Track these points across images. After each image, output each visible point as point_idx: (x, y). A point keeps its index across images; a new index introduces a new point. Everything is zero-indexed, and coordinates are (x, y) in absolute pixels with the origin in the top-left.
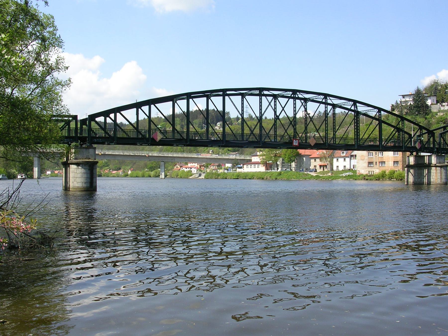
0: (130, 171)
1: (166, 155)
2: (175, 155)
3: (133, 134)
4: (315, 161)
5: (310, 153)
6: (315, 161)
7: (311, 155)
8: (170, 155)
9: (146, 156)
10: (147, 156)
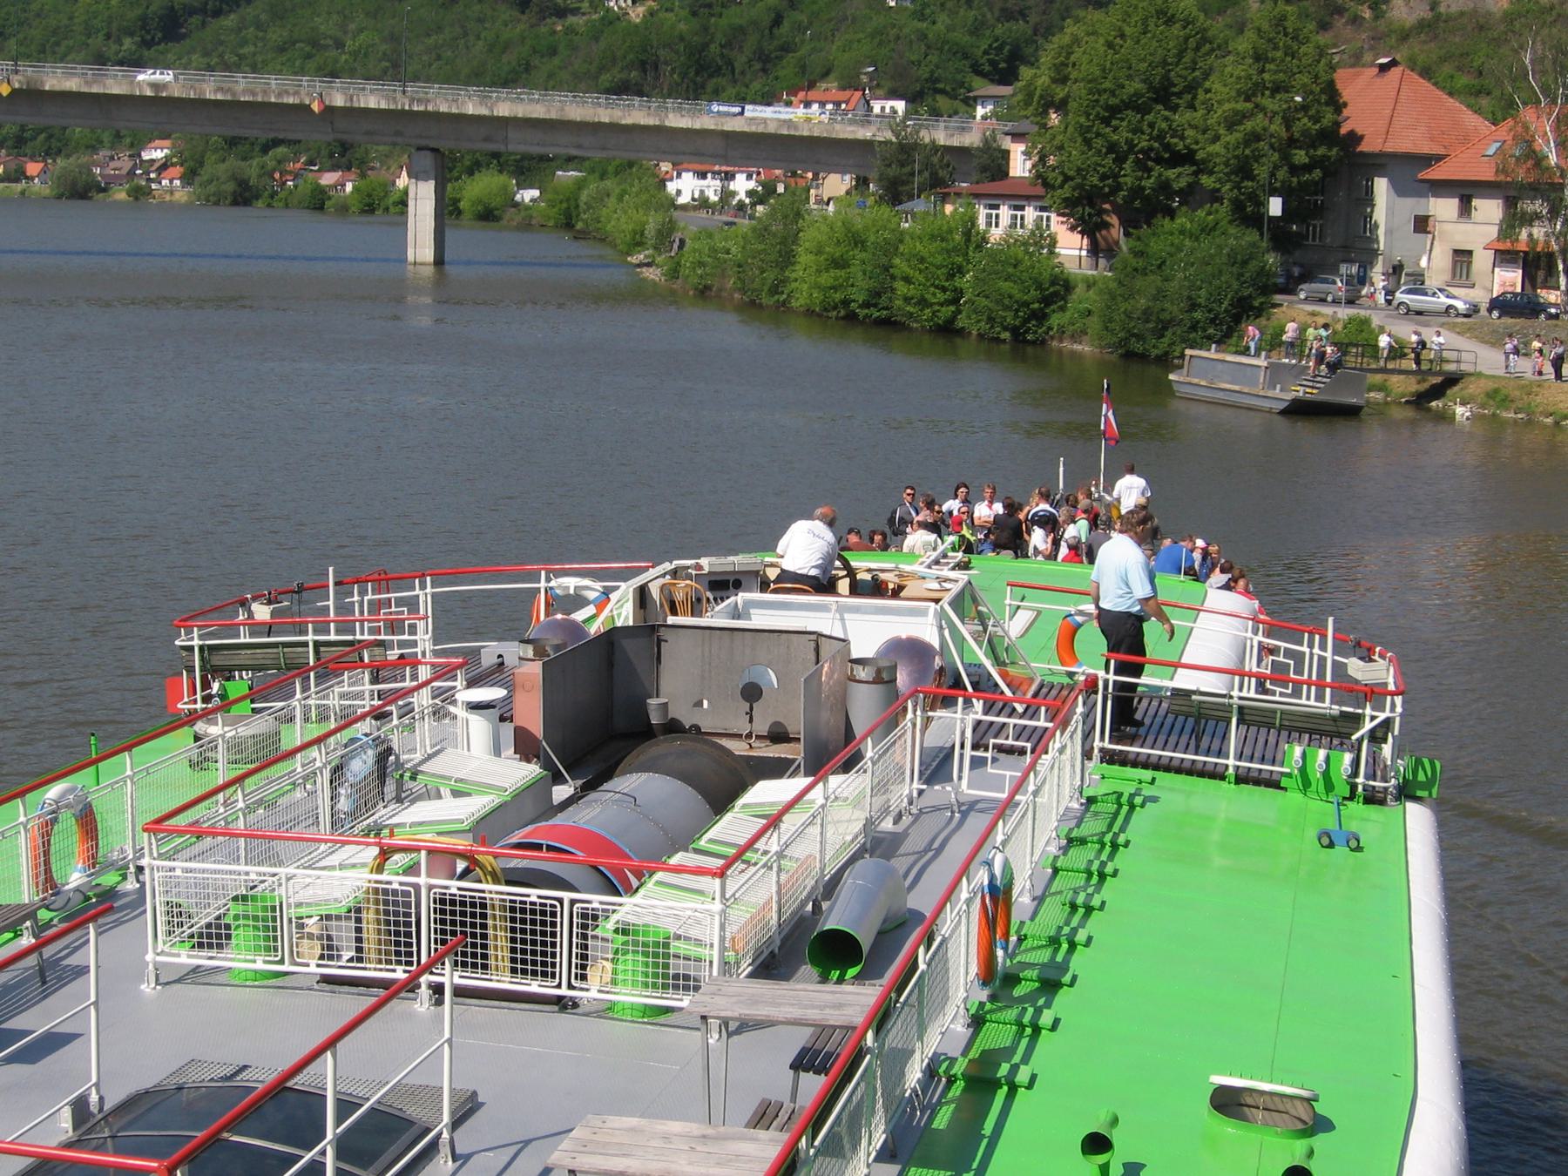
0: (404, 173)
1: (443, 108)
2: (504, 109)
3: (1310, 384)
4: (1465, 210)
5: (1432, 139)
6: (1465, 210)
7: (1439, 158)
8: (471, 108)
9: (308, 108)
10: (315, 107)
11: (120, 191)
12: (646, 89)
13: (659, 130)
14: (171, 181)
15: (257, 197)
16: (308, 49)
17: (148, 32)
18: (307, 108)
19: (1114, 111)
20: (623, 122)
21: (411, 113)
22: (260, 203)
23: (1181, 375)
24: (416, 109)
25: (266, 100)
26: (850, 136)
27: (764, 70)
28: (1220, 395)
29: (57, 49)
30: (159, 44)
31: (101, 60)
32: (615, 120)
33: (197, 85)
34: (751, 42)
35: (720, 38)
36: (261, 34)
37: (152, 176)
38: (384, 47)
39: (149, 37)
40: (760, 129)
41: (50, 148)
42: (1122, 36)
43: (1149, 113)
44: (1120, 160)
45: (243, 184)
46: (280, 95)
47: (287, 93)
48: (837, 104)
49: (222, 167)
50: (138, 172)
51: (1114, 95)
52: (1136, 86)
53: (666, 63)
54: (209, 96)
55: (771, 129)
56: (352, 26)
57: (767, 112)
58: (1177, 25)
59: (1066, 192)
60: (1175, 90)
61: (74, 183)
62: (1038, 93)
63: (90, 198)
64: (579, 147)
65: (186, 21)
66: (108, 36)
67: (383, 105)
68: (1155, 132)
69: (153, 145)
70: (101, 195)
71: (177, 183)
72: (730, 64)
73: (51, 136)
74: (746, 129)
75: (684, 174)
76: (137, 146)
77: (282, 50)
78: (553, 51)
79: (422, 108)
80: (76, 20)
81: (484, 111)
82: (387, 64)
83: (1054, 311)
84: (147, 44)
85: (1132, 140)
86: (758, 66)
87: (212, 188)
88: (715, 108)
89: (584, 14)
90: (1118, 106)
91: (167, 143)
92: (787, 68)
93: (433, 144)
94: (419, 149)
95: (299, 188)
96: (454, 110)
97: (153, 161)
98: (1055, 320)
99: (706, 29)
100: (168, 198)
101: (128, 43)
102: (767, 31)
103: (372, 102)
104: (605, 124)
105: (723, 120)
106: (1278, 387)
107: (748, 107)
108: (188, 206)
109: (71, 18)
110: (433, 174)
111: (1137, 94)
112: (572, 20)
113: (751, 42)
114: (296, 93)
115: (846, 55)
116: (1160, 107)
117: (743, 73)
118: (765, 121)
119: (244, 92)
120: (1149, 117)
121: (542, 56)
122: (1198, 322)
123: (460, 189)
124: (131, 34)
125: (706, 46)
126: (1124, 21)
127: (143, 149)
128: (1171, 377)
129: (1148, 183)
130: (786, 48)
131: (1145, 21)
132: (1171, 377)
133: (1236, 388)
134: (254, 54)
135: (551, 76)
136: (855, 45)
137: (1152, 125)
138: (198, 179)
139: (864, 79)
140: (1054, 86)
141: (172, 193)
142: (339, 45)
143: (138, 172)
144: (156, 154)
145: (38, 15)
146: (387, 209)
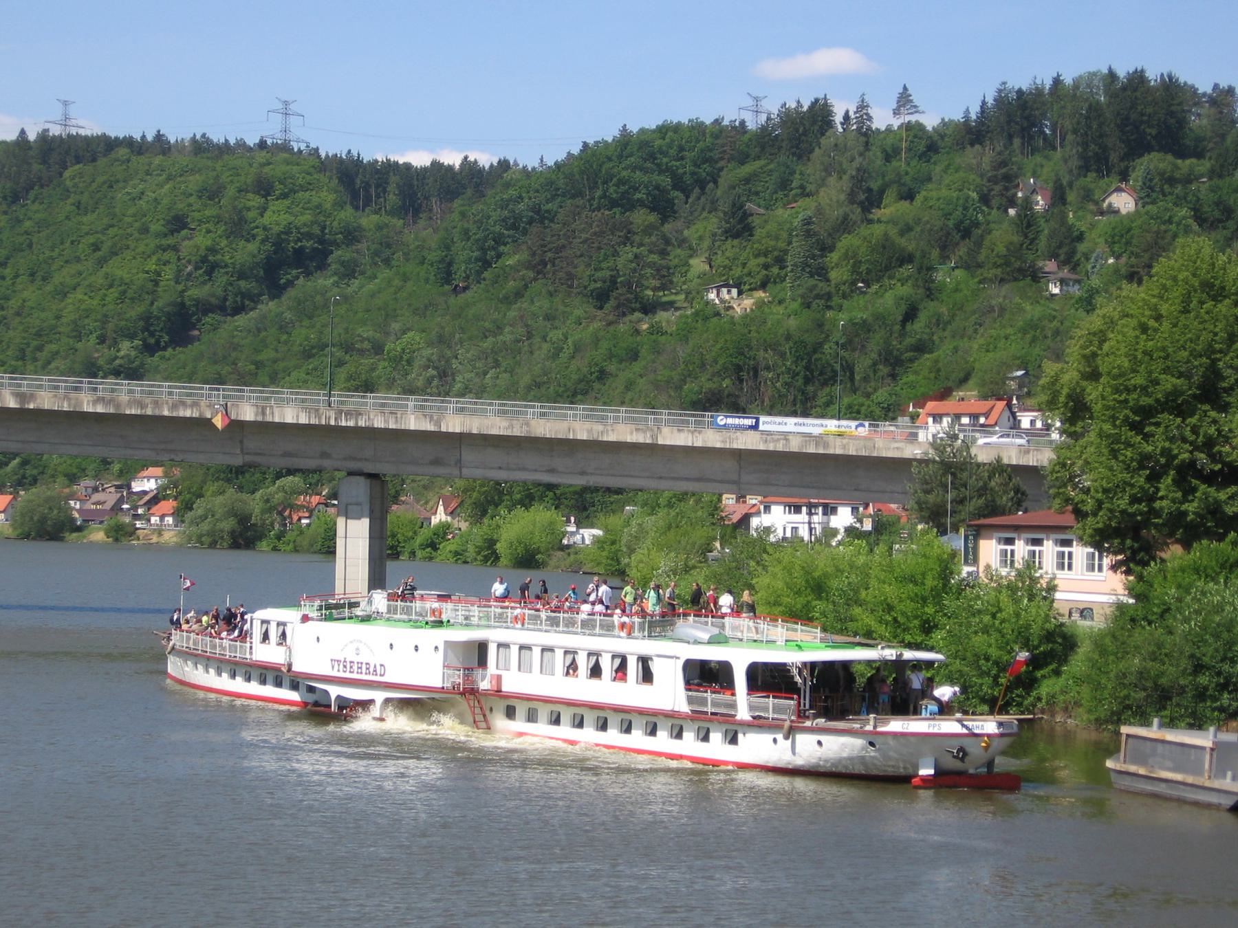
1: (379, 423)
2: (454, 424)
8: (413, 422)
10: (218, 422)
11: (99, 529)
12: (742, 401)
13: (652, 449)
14: (162, 517)
15: (261, 537)
16: (339, 354)
17: (152, 334)
18: (208, 423)
19: (1147, 413)
20: (605, 439)
21: (338, 430)
22: (264, 545)
23: (1118, 760)
24: (344, 424)
25: (157, 413)
26: (890, 454)
27: (893, 376)
28: (1161, 788)
29: (38, 354)
30: (165, 349)
31: (91, 370)
32: (595, 437)
33: (73, 395)
34: (875, 343)
35: (837, 336)
36: (284, 337)
37: (140, 511)
38: (427, 352)
39: (152, 341)
40: (780, 447)
41: (24, 477)
42: (1158, 318)
43: (1191, 416)
44: (1154, 477)
45: (243, 519)
46: (174, 407)
47: (184, 404)
48: (975, 417)
49: (220, 499)
50: (125, 506)
51: (1148, 395)
52: (1169, 382)
53: (768, 368)
54: (87, 408)
55: (794, 446)
56: (396, 326)
57: (790, 424)
58: (1227, 301)
59: (1098, 522)
60: (1225, 385)
61: (43, 520)
62: (1065, 391)
63: (61, 539)
64: (552, 471)
65: (199, 320)
66: (102, 340)
67: (303, 420)
68: (1201, 439)
69: (145, 473)
70: (75, 535)
71: (169, 520)
72: (849, 369)
73: (25, 463)
74: (762, 447)
75: (774, 508)
76: (129, 472)
77: (308, 354)
78: (634, 356)
79: (351, 423)
80: (64, 320)
81: (429, 427)
82: (434, 373)
83: (1044, 677)
84: (150, 349)
85: (1170, 450)
86: (884, 370)
87: (205, 527)
88: (721, 420)
89: (677, 309)
90: (1150, 406)
91: (159, 471)
92: (918, 374)
93: (369, 468)
94: (351, 473)
95: (313, 526)
96: (392, 425)
97: (145, 493)
98: (1046, 688)
99: (820, 325)
100: (155, 539)
101: (126, 347)
102: (897, 327)
103: (290, 415)
104: (361, 428)
105: (733, 435)
106: (1229, 774)
107: (762, 419)
108: (179, 546)
109: (58, 317)
110: (366, 508)
111: (1176, 392)
112: (662, 316)
113: (875, 343)
114: (195, 405)
115: (991, 355)
116: (1207, 407)
117: (866, 379)
118: (785, 435)
119: (130, 404)
120: (1193, 420)
121: (621, 361)
122: (1206, 688)
123: (498, 526)
124: (131, 337)
125: (818, 347)
126: (1161, 297)
127: (134, 478)
128: (1109, 764)
129: (1191, 507)
130: (921, 348)
131: (1187, 300)
132: (1109, 764)
133: (1178, 777)
134: (275, 361)
135: (629, 386)
136: (1001, 344)
137: (1195, 430)
138: (189, 515)
139: (1013, 385)
140: (1084, 383)
141: (160, 533)
142: (378, 349)
143: (125, 506)
144: (146, 484)
145: (18, 314)
146: (413, 553)
